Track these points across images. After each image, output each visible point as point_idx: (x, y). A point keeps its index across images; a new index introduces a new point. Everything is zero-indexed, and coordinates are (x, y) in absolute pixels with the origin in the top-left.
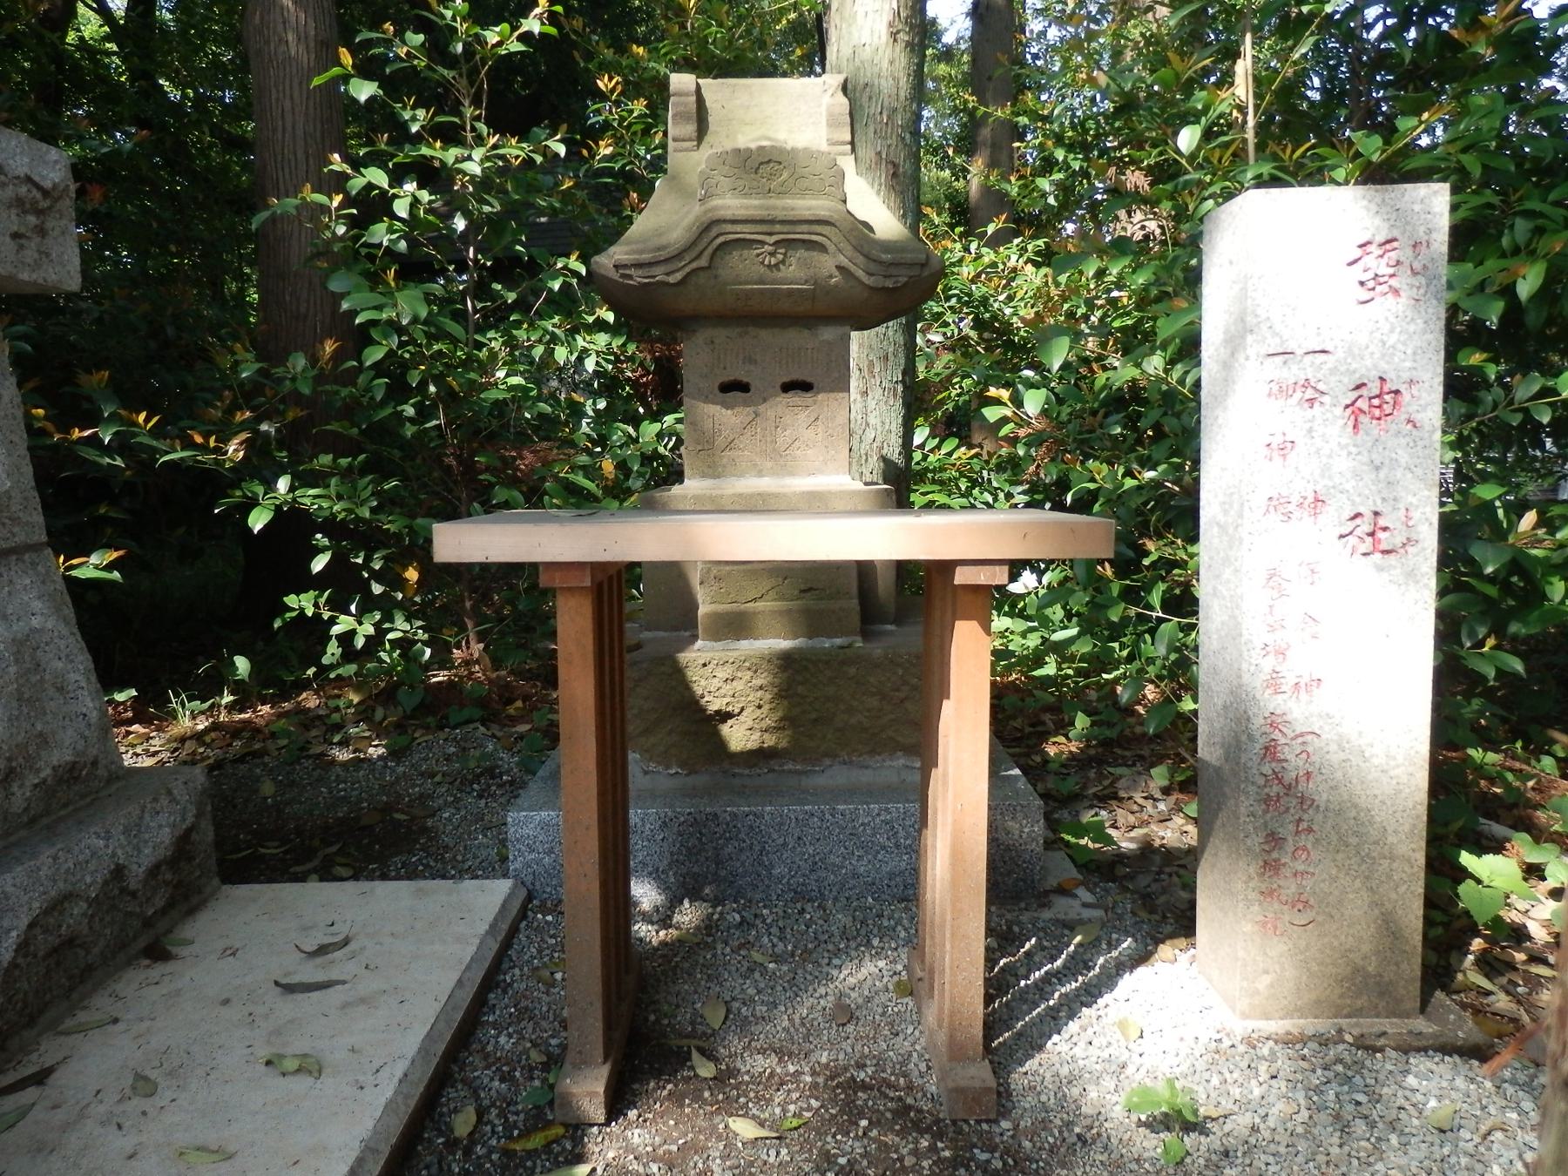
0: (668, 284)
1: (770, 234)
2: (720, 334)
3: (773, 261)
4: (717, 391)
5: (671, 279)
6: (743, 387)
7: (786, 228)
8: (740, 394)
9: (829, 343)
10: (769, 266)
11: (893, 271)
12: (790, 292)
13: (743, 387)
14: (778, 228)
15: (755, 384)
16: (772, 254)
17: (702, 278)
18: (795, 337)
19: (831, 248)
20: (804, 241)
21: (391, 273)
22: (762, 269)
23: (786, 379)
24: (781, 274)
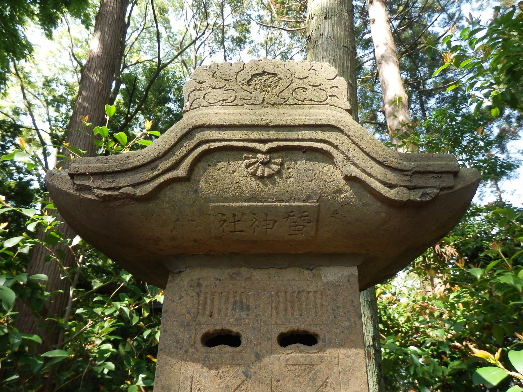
0: (133, 198)
1: (264, 141)
2: (209, 276)
3: (267, 172)
4: (199, 345)
5: (140, 192)
6: (232, 339)
7: (282, 135)
8: (228, 348)
9: (332, 284)
10: (262, 178)
11: (419, 181)
12: (289, 212)
13: (232, 339)
14: (273, 134)
15: (246, 335)
16: (265, 164)
17: (178, 192)
18: (292, 279)
19: (339, 157)
20: (305, 150)
21: (122, 324)
22: (255, 183)
23: (284, 329)
24: (276, 189)
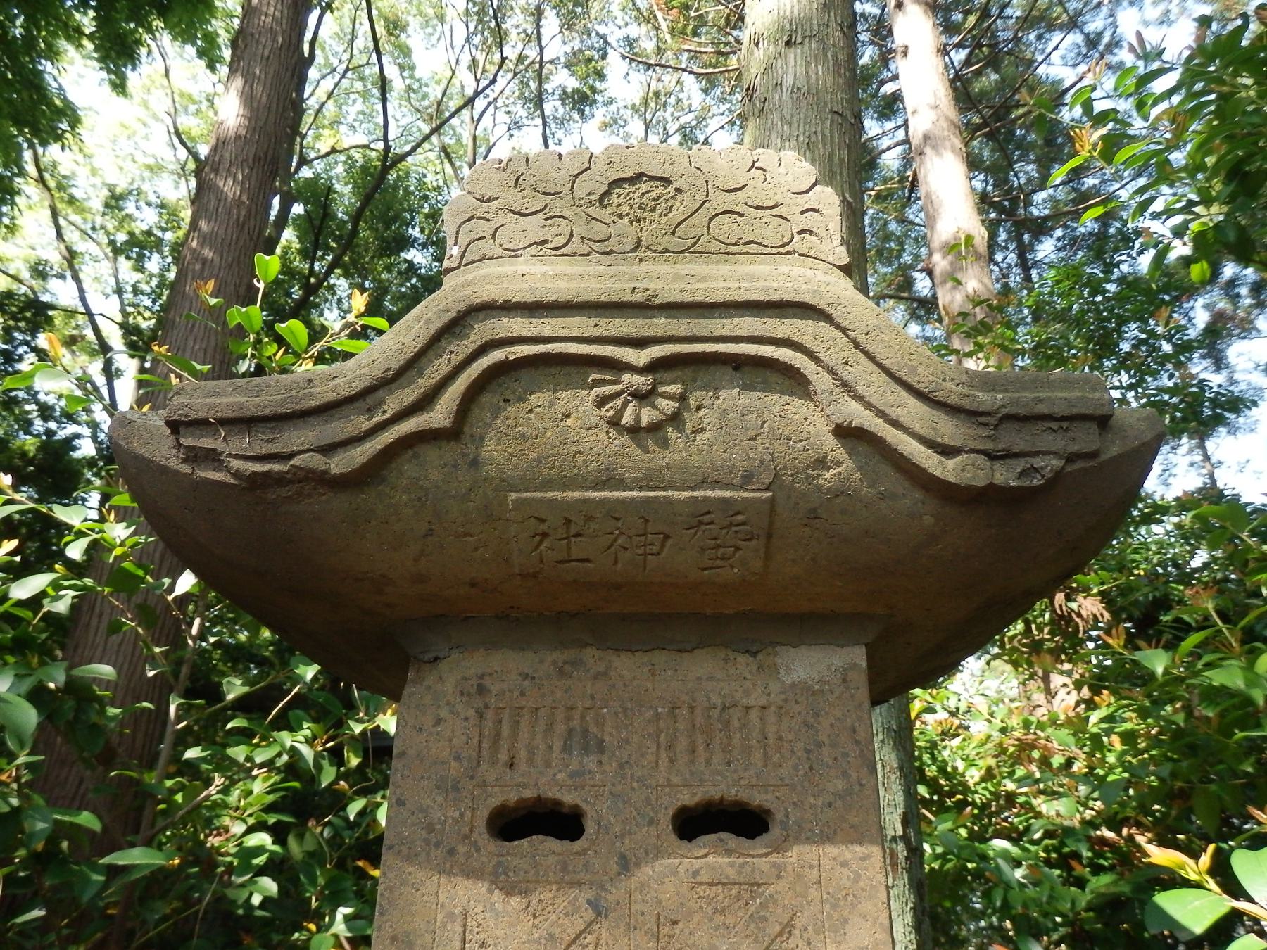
0: (323, 480)
1: (640, 343)
2: (507, 668)
3: (647, 416)
4: (482, 835)
5: (338, 464)
6: (562, 823)
7: (683, 326)
8: (552, 843)
9: (805, 688)
10: (634, 431)
11: (1015, 439)
12: (701, 514)
13: (562, 823)
14: (661, 325)
15: (596, 812)
16: (643, 397)
17: (432, 466)
18: (708, 676)
19: (820, 380)
20: (738, 363)
21: (296, 784)
22: (617, 442)
23: (688, 798)
24: (669, 457)
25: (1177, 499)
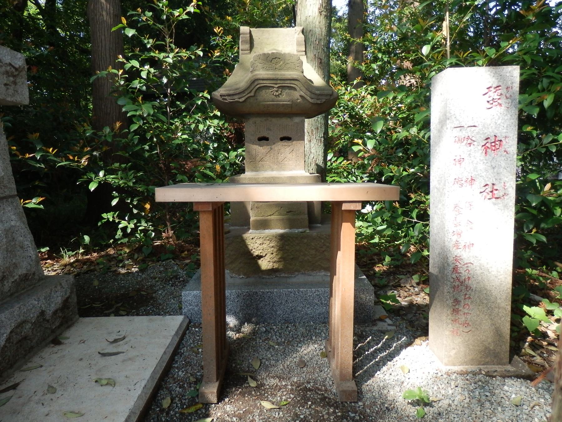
0: (239, 102)
1: (276, 84)
2: (258, 120)
3: (277, 94)
4: (257, 140)
5: (241, 100)
6: (266, 139)
7: (282, 82)
8: (265, 141)
9: (297, 123)
10: (276, 95)
11: (320, 97)
12: (283, 105)
13: (266, 139)
14: (279, 82)
15: (271, 138)
16: (277, 91)
17: (252, 100)
18: (285, 121)
19: (298, 89)
20: (288, 86)
22: (273, 97)
23: (282, 136)
24: (280, 98)
25: (198, 221)
